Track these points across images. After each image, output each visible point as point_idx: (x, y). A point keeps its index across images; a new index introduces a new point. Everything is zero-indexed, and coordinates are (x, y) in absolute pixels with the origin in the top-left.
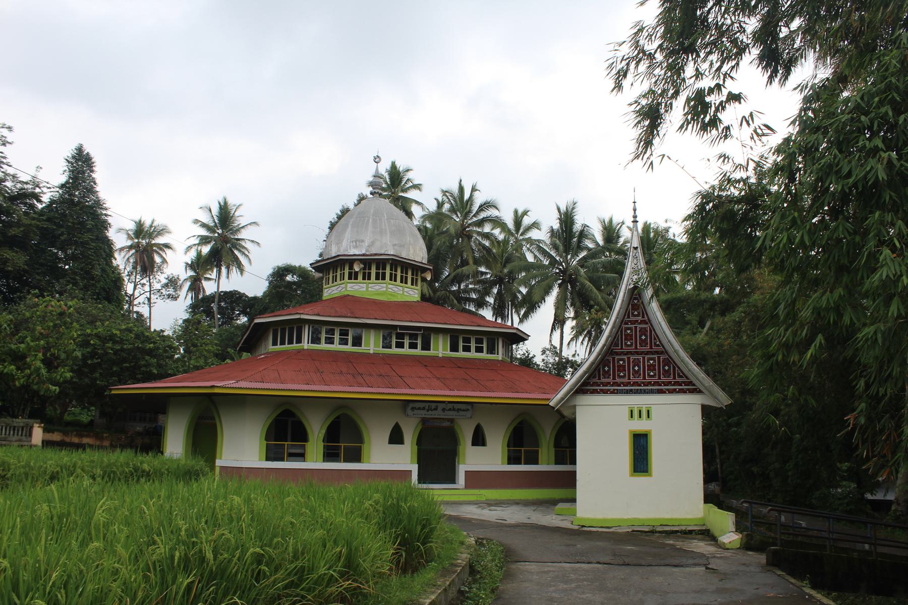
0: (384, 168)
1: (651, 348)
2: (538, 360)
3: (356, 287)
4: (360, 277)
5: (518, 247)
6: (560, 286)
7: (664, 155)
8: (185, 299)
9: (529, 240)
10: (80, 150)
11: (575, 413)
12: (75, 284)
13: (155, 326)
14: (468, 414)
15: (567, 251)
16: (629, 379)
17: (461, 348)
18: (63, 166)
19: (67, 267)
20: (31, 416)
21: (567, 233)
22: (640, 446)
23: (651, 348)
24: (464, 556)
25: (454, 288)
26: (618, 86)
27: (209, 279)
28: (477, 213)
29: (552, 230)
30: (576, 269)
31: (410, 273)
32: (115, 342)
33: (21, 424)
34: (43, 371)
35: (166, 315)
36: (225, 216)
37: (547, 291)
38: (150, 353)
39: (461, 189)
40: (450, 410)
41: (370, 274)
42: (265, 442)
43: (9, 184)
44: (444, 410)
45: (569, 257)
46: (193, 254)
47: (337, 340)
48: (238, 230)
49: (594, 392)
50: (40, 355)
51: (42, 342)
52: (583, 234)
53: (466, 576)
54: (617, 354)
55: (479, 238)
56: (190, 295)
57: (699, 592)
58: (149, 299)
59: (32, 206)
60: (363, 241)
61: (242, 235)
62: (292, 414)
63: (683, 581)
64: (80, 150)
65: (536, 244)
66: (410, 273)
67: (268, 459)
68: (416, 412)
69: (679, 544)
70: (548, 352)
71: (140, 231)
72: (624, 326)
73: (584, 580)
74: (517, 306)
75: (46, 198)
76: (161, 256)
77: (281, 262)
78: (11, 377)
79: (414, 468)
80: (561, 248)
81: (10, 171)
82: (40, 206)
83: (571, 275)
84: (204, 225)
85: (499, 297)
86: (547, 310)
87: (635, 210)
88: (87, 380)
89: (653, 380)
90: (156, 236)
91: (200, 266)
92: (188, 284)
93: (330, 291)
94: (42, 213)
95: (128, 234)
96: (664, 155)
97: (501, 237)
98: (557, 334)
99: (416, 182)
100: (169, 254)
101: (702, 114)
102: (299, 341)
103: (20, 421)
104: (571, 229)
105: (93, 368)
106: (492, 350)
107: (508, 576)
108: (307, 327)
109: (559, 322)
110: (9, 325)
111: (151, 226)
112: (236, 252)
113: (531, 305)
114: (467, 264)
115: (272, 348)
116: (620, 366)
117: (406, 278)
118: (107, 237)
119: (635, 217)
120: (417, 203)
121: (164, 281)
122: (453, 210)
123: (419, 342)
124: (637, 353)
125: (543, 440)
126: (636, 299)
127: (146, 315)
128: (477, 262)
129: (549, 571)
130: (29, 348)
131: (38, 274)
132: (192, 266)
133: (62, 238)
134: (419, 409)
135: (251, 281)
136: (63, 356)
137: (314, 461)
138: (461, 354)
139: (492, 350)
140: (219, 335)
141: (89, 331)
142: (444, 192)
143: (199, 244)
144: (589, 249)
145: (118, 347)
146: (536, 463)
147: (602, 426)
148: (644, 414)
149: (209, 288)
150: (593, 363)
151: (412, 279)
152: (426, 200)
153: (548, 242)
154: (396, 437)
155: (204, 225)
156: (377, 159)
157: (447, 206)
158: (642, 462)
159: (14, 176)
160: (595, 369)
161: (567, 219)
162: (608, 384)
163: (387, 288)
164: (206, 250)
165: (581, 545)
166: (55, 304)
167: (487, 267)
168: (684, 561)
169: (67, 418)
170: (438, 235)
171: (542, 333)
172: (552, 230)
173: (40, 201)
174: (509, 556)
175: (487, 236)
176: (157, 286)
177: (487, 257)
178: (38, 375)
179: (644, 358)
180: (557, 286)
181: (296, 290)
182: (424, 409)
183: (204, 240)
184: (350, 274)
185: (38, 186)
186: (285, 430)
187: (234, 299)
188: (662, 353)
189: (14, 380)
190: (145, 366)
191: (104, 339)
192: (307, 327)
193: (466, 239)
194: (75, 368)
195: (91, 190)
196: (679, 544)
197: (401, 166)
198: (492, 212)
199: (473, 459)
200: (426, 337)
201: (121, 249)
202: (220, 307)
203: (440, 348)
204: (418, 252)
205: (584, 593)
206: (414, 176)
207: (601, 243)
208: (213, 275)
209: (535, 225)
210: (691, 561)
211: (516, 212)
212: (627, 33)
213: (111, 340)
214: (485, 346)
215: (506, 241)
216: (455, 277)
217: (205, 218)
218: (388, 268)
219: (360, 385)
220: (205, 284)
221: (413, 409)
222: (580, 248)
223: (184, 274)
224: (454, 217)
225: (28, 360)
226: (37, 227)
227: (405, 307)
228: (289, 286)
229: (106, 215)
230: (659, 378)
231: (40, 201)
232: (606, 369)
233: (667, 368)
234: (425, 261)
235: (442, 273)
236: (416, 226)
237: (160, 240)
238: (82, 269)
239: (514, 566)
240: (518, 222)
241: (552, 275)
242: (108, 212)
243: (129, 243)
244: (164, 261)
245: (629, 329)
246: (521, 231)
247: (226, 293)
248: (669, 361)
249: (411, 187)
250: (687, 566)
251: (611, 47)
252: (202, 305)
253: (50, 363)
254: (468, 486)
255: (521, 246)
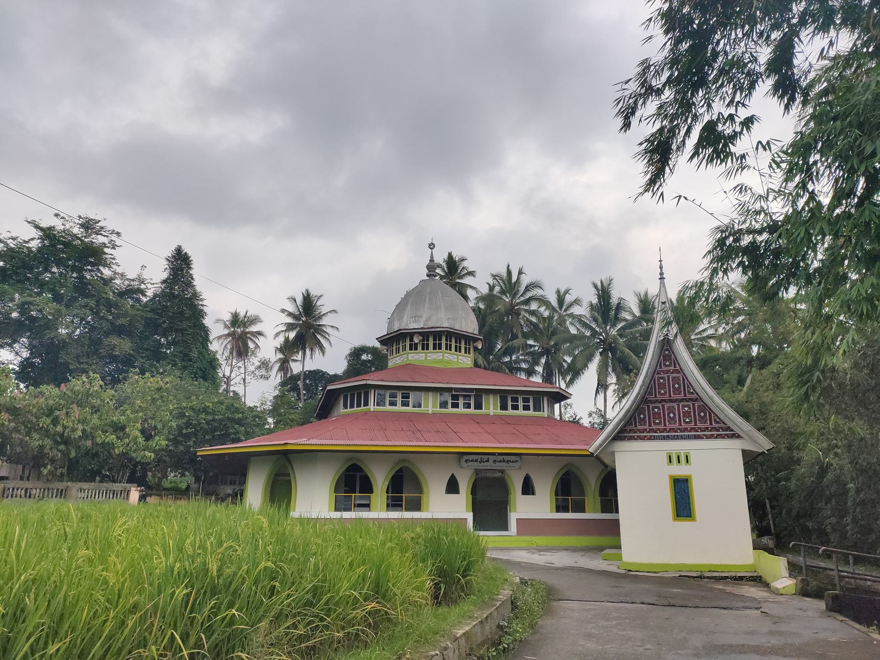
0: (440, 258)
1: (685, 395)
2: (586, 422)
3: (417, 357)
4: (420, 347)
5: (562, 322)
6: (601, 354)
7: (680, 196)
8: (276, 378)
9: (571, 315)
10: (179, 250)
11: (614, 462)
12: (175, 365)
13: (250, 403)
14: (517, 465)
15: (605, 323)
16: (665, 425)
17: (510, 407)
18: (164, 264)
19: (168, 352)
20: (130, 481)
21: (605, 307)
22: (681, 491)
23: (685, 395)
24: (506, 592)
25: (507, 359)
26: (627, 125)
27: (296, 361)
28: (524, 293)
29: (591, 305)
30: (614, 337)
31: (463, 343)
32: (207, 413)
33: (120, 489)
34: (141, 440)
35: (257, 390)
36: (308, 305)
37: (590, 358)
38: (239, 422)
39: (509, 273)
40: (500, 461)
41: (428, 344)
42: (334, 495)
43: (118, 281)
44: (495, 461)
45: (608, 327)
46: (281, 339)
47: (399, 402)
48: (320, 317)
49: (631, 438)
50: (139, 425)
51: (141, 414)
52: (619, 307)
53: (507, 611)
54: (651, 402)
55: (527, 315)
56: (279, 375)
57: (749, 633)
58: (244, 380)
59: (138, 300)
60: (421, 316)
61: (324, 321)
62: (360, 469)
63: (734, 626)
64: (179, 250)
65: (579, 319)
66: (463, 343)
67: (336, 509)
68: (469, 464)
69: (729, 589)
70: (594, 415)
71: (236, 320)
72: (656, 376)
73: (626, 618)
74: (563, 374)
75: (150, 293)
76: (255, 342)
77: (358, 343)
78: (112, 445)
79: (470, 516)
80: (600, 319)
81: (119, 270)
82: (145, 300)
83: (610, 344)
84: (290, 314)
85: (547, 366)
86: (590, 375)
87: (661, 268)
88: (182, 448)
89: (689, 426)
90: (250, 325)
91: (288, 349)
92: (277, 366)
93: (394, 361)
94: (146, 305)
95: (225, 324)
96: (680, 196)
97: (546, 314)
98: (601, 397)
99: (470, 270)
100: (261, 341)
101: (716, 144)
102: (366, 404)
103: (118, 487)
104: (609, 303)
105: (187, 437)
106: (537, 408)
107: (548, 611)
108: (373, 391)
109: (602, 386)
110: (111, 400)
111: (245, 317)
112: (319, 337)
113: (575, 371)
114: (517, 337)
115: (342, 411)
116: (655, 414)
117: (460, 347)
118: (203, 324)
119: (662, 274)
120: (471, 287)
121: (258, 364)
122: (503, 292)
123: (472, 402)
124: (671, 401)
125: (586, 487)
126: (667, 350)
127: (241, 393)
128: (526, 336)
129: (591, 609)
130: (129, 420)
131: (142, 357)
132: (282, 349)
133: (164, 326)
134: (472, 461)
135: (331, 360)
136: (159, 426)
137: (378, 511)
138: (510, 412)
139: (537, 408)
140: (304, 408)
141: (184, 404)
142: (494, 277)
143: (286, 331)
144: (625, 320)
145: (210, 417)
146: (583, 511)
147: (642, 471)
148: (683, 459)
149: (296, 368)
150: (628, 411)
151: (466, 348)
152: (479, 285)
153: (588, 316)
154: (452, 487)
155: (290, 314)
156: (432, 246)
157: (497, 289)
158: (687, 509)
159: (122, 275)
160: (631, 418)
161: (604, 293)
162: (644, 431)
163: (443, 356)
164: (292, 335)
165: (629, 587)
166: (153, 381)
167: (535, 340)
168: (734, 604)
169: (166, 484)
170: (490, 314)
171: (590, 400)
172: (591, 305)
173: (145, 295)
174: (550, 595)
175: (533, 313)
176: (252, 368)
177: (535, 332)
178: (136, 443)
179: (678, 405)
180: (598, 354)
181: (370, 367)
182: (476, 461)
183: (290, 327)
184: (411, 345)
185: (143, 282)
186: (353, 483)
187: (317, 376)
188: (696, 400)
189: (114, 449)
190: (234, 434)
191: (197, 412)
192: (373, 391)
193: (515, 316)
194: (172, 437)
195: (189, 284)
196: (729, 589)
197: (456, 256)
198: (537, 292)
199: (525, 508)
200: (478, 397)
201: (219, 337)
202: (305, 385)
203: (491, 407)
204: (470, 325)
205: (624, 630)
206: (469, 265)
207: (638, 314)
208: (299, 356)
209: (577, 302)
210: (741, 604)
211: (558, 292)
212: (634, 70)
213: (203, 411)
214: (531, 404)
215: (550, 318)
216: (506, 349)
217: (291, 308)
218: (444, 339)
219: (418, 440)
220: (292, 364)
221: (466, 461)
222: (617, 319)
223: (274, 357)
224: (504, 297)
225: (127, 430)
226: (142, 317)
227: (461, 372)
228: (360, 361)
229: (202, 305)
230: (696, 424)
231: (145, 295)
232: (642, 416)
233: (702, 414)
234: (476, 332)
235: (495, 347)
236: (472, 308)
237: (254, 328)
238: (181, 352)
239: (555, 604)
240: (561, 301)
241: (593, 345)
242: (205, 303)
243: (226, 332)
244: (257, 346)
245: (662, 378)
246: (564, 307)
247: (310, 371)
248: (704, 407)
249: (466, 274)
250: (737, 609)
251: (619, 87)
252: (290, 383)
253: (147, 435)
254: (520, 532)
255: (565, 321)
